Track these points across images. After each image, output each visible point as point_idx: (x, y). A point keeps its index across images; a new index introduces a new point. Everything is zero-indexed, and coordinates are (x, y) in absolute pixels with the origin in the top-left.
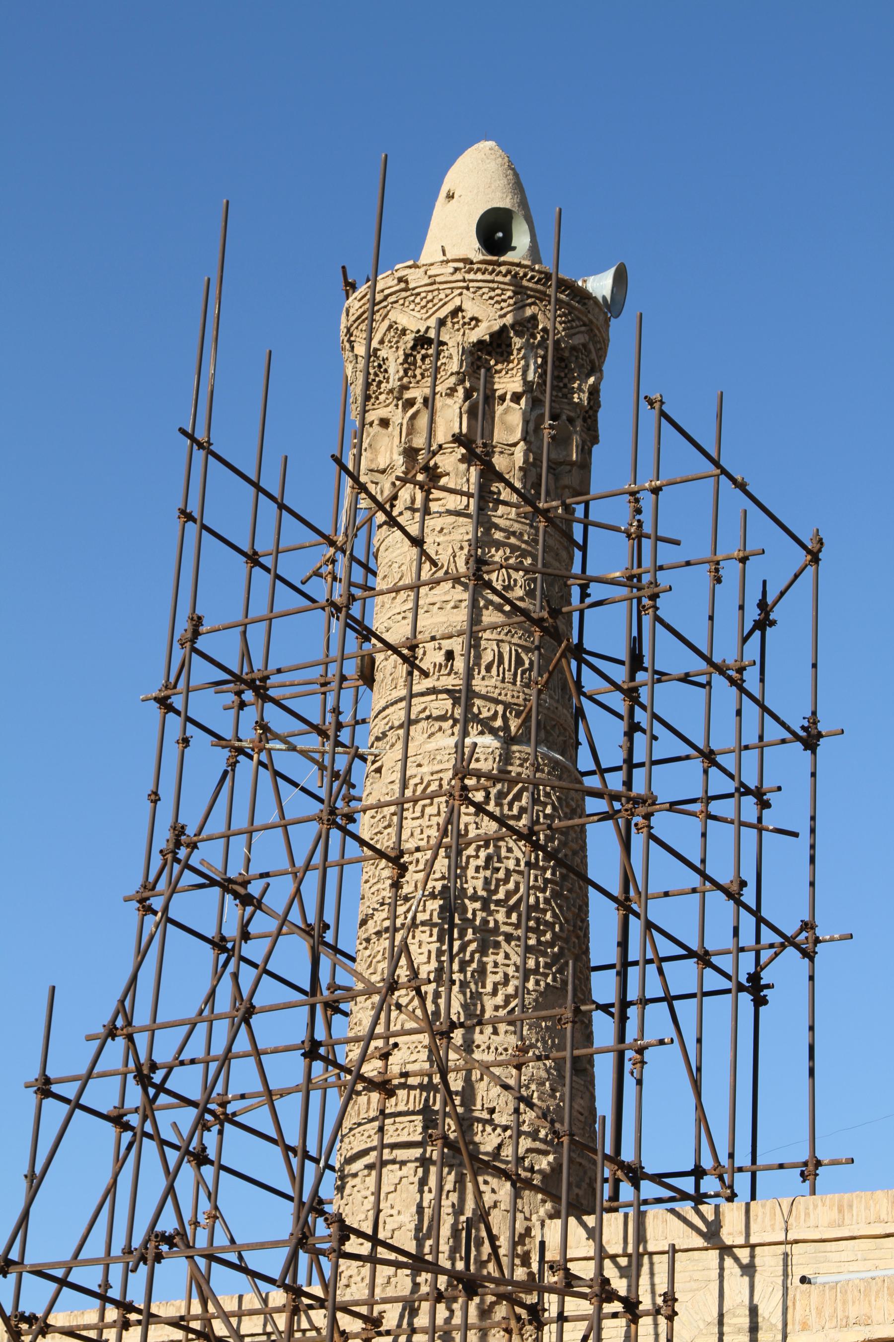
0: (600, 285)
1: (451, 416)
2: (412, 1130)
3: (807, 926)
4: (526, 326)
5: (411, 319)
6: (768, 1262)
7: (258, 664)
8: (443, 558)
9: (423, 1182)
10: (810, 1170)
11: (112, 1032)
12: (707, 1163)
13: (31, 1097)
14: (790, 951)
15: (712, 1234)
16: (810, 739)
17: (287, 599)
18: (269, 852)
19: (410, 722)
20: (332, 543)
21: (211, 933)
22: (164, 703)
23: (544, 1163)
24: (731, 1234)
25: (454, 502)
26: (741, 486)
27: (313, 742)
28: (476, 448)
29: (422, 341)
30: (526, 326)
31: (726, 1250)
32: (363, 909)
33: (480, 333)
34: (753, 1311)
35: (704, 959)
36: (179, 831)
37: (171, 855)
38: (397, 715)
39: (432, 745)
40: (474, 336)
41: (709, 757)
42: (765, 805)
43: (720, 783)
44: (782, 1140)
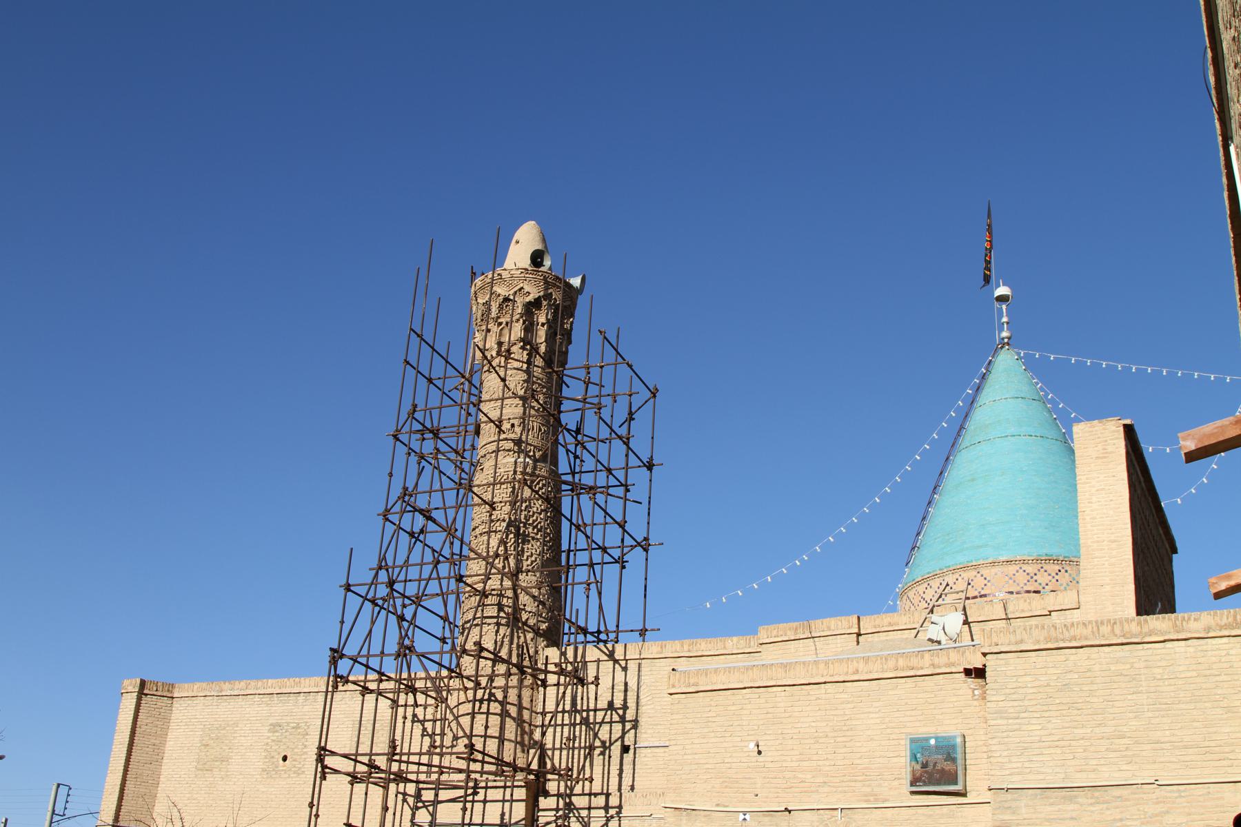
0: (576, 282)
1: (518, 330)
2: (492, 611)
3: (646, 539)
4: (548, 296)
5: (502, 290)
6: (632, 666)
7: (435, 424)
8: (512, 386)
9: (497, 631)
10: (643, 632)
11: (380, 568)
12: (602, 629)
13: (342, 591)
14: (639, 548)
15: (611, 655)
16: (650, 466)
17: (447, 401)
18: (436, 500)
19: (497, 451)
20: (463, 377)
21: (409, 530)
22: (396, 437)
23: (544, 626)
24: (619, 655)
25: (517, 365)
26: (630, 366)
27: (453, 456)
28: (527, 341)
29: (506, 299)
30: (548, 296)
31: (616, 661)
32: (474, 524)
33: (530, 298)
34: (626, 684)
35: (604, 550)
36: (405, 489)
37: (402, 498)
38: (493, 447)
39: (505, 461)
40: (528, 299)
41: (609, 471)
42: (628, 490)
43: (613, 481)
44: (631, 620)
